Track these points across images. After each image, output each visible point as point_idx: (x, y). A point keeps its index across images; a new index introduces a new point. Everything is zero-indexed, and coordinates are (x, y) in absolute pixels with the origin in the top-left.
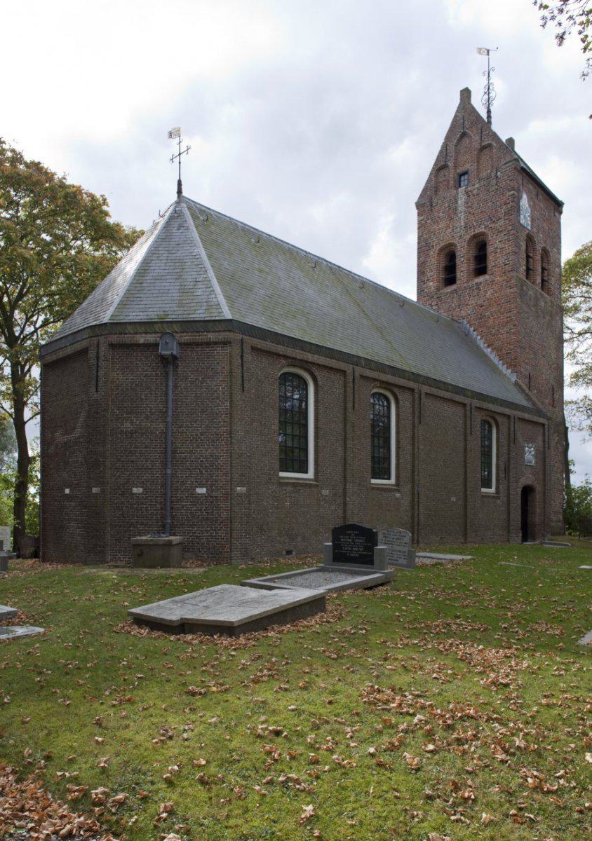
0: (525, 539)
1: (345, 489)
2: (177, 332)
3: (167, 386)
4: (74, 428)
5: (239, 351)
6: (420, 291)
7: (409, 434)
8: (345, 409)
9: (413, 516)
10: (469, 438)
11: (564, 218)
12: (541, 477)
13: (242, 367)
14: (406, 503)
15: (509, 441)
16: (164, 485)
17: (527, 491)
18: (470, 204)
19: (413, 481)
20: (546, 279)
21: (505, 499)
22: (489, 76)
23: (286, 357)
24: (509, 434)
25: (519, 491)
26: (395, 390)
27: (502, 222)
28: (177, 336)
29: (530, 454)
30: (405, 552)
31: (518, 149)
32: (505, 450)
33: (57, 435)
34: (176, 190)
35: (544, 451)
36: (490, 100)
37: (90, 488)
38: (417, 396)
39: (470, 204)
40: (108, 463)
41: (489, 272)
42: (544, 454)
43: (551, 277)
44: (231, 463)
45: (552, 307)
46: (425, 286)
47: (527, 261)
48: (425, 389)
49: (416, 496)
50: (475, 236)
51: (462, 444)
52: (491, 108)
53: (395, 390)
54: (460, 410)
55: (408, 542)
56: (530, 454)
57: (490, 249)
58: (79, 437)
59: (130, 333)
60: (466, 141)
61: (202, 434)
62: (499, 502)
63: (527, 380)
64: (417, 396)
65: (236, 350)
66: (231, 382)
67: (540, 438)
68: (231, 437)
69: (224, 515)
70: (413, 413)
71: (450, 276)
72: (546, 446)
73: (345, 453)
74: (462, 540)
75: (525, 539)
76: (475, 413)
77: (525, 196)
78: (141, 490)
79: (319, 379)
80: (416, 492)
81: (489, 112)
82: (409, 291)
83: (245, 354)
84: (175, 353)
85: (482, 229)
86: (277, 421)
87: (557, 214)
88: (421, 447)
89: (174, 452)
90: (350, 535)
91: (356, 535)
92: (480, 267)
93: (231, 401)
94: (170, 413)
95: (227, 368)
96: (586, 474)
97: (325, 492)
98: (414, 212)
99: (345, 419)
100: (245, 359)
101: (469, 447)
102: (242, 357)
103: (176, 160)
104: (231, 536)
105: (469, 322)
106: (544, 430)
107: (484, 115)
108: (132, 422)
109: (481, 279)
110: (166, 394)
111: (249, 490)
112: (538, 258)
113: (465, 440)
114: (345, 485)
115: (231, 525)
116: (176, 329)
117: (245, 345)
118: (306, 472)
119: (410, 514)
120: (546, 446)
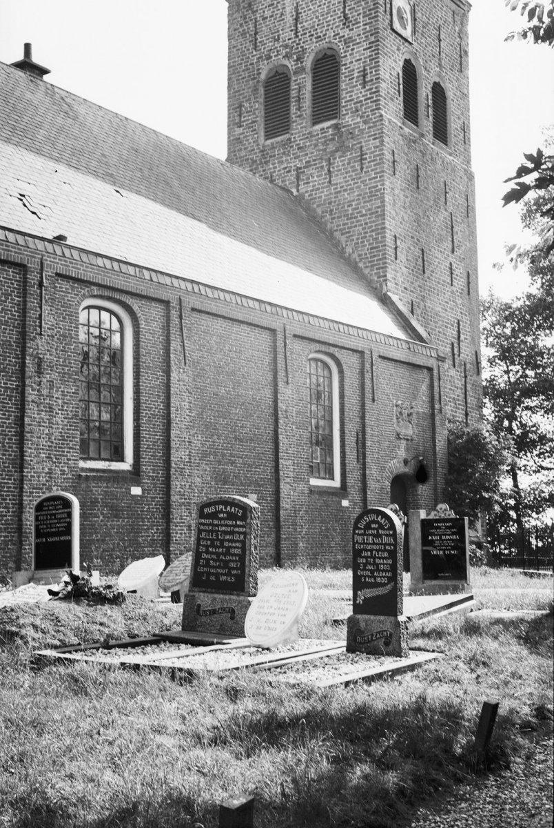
6: (234, 143)
26: (130, 301)
53: (130, 301)
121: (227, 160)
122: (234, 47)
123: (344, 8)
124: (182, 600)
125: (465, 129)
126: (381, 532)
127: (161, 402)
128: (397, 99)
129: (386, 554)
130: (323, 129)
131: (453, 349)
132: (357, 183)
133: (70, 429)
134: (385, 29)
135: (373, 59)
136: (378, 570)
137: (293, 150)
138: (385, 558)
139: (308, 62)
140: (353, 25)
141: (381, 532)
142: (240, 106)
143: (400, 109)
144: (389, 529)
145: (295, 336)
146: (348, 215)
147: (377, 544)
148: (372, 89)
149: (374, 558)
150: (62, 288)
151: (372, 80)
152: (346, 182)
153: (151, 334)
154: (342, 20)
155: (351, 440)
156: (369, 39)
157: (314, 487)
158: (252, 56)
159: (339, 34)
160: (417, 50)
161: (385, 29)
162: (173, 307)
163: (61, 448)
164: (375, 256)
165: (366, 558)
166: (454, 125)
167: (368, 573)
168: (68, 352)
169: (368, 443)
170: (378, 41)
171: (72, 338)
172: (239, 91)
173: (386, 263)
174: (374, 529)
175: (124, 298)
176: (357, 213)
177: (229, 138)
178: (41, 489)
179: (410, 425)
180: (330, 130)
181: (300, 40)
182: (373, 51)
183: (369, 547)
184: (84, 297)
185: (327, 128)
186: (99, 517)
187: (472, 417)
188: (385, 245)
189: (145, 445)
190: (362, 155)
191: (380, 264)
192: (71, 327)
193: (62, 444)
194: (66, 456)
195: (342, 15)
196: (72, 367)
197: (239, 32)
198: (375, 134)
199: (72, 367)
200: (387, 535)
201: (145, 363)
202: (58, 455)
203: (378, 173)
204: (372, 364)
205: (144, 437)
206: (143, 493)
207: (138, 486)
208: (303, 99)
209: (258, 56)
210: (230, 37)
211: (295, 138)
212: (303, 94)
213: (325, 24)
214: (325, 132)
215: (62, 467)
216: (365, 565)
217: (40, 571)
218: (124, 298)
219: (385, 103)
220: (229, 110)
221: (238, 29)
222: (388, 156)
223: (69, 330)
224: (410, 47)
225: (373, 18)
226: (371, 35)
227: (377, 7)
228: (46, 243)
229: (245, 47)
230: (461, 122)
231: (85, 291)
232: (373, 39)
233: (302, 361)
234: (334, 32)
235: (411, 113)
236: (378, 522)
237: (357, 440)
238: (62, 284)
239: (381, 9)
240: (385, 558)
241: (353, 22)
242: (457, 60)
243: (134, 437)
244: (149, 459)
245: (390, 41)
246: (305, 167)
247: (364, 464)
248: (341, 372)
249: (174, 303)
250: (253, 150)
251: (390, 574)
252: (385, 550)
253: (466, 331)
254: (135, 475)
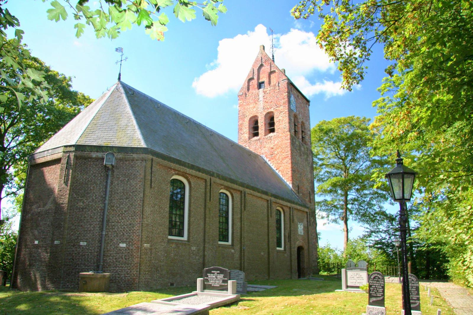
0: (299, 277)
1: (204, 247)
2: (115, 153)
3: (107, 182)
4: (46, 204)
5: (150, 165)
7: (239, 216)
8: (205, 201)
9: (241, 263)
10: (270, 218)
11: (311, 108)
12: (307, 241)
13: (151, 174)
14: (237, 256)
15: (290, 221)
16: (100, 241)
17: (300, 249)
18: (265, 97)
19: (241, 243)
20: (304, 136)
21: (289, 254)
23: (175, 170)
24: (290, 218)
25: (296, 249)
27: (282, 108)
28: (115, 155)
29: (301, 228)
30: (241, 284)
32: (288, 226)
33: (34, 207)
34: (118, 78)
35: (308, 226)
37: (53, 241)
38: (243, 195)
39: (265, 97)
40: (66, 226)
41: (276, 131)
42: (308, 228)
43: (306, 136)
44: (142, 229)
45: (307, 151)
46: (242, 136)
47: (295, 127)
48: (247, 191)
49: (243, 251)
50: (268, 113)
51: (266, 222)
55: (243, 277)
56: (301, 228)
57: (276, 120)
58: (49, 210)
59: (88, 151)
60: (263, 68)
61: (125, 211)
62: (286, 255)
63: (297, 188)
64: (243, 195)
65: (149, 163)
66: (145, 182)
67: (305, 220)
68: (143, 214)
69: (136, 260)
70: (241, 204)
72: (309, 224)
73: (205, 225)
74: (267, 277)
75: (299, 277)
77: (292, 96)
78: (85, 243)
80: (243, 250)
81: (273, 56)
83: (153, 167)
84: (113, 164)
85: (272, 110)
86: (168, 206)
87: (307, 106)
88: (245, 224)
89: (108, 221)
90: (214, 273)
91: (218, 273)
92: (271, 126)
93: (144, 194)
94: (107, 198)
95: (143, 174)
96: (75, 77)
97: (194, 248)
99: (205, 206)
100: (153, 170)
101: (270, 224)
102: (151, 168)
103: (120, 63)
104: (140, 273)
105: (266, 156)
106: (307, 215)
108: (83, 202)
109: (272, 134)
110: (106, 187)
111: (151, 246)
112: (300, 126)
113: (268, 220)
114: (204, 245)
115: (140, 267)
116: (115, 151)
117: (153, 162)
118: (183, 236)
119: (239, 262)
120: (309, 224)
124: (223, 284)
126: (379, 280)
129: (381, 287)
136: (378, 292)
141: (379, 280)
144: (382, 279)
149: (377, 288)
183: (375, 284)
204: (210, 185)
216: (373, 290)
248: (284, 211)
251: (382, 294)
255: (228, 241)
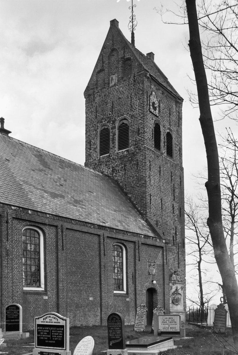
6: (88, 156)
22: (132, 10)
26: (42, 226)
31: (156, 61)
36: (134, 26)
52: (134, 31)
53: (42, 226)
54: (96, 239)
71: (105, 148)
76: (109, 241)
79: (46, 231)
81: (133, 34)
82: (80, 158)
98: (83, 100)
107: (129, 40)
121: (86, 165)
122: (88, 117)
123: (131, 103)
125: (180, 150)
127: (55, 264)
128: (152, 140)
130: (123, 152)
131: (173, 238)
132: (135, 174)
133: (19, 276)
134: (147, 111)
135: (142, 124)
136: (116, 334)
137: (111, 160)
138: (119, 330)
139: (117, 125)
140: (134, 110)
141: (117, 321)
142: (90, 142)
143: (153, 144)
145: (108, 237)
146: (132, 186)
147: (115, 325)
148: (141, 136)
150: (15, 223)
151: (141, 132)
152: (131, 173)
153: (51, 238)
154: (130, 108)
155: (130, 276)
156: (140, 116)
157: (115, 293)
158: (95, 121)
159: (129, 113)
160: (160, 119)
161: (147, 111)
162: (59, 228)
163: (16, 283)
164: (142, 203)
165: (112, 330)
166: (175, 149)
167: (113, 335)
168: (18, 247)
169: (137, 277)
170: (144, 116)
171: (19, 241)
172: (90, 135)
173: (146, 205)
174: (114, 320)
175: (39, 225)
176: (136, 186)
177: (86, 154)
178: (9, 298)
179: (154, 269)
180: (125, 152)
181: (114, 115)
182: (142, 121)
184: (24, 226)
185: (124, 151)
186: (31, 308)
187: (181, 264)
188: (146, 199)
189: (49, 280)
190: (137, 163)
191: (144, 206)
192: (19, 237)
193: (17, 281)
194: (18, 286)
195: (130, 105)
196: (20, 252)
197: (90, 111)
198: (143, 154)
199: (20, 252)
200: (118, 322)
201: (48, 249)
202: (15, 285)
203: (144, 170)
205: (48, 278)
206: (48, 298)
207: (46, 296)
208: (115, 139)
209: (97, 121)
210: (86, 113)
211: (111, 155)
212: (115, 138)
213: (124, 109)
214: (123, 153)
215: (17, 290)
217: (7, 332)
218: (39, 225)
219: (147, 142)
220: (86, 143)
221: (90, 110)
222: (148, 163)
223: (18, 238)
224: (157, 118)
225: (142, 107)
226: (141, 114)
227: (144, 103)
228: (8, 206)
229: (92, 117)
230: (179, 148)
231: (24, 223)
232: (142, 116)
233: (110, 246)
234: (127, 112)
235: (157, 145)
236: (115, 318)
237: (133, 276)
238: (15, 221)
239: (145, 103)
240: (119, 330)
241: (134, 109)
242: (177, 122)
243: (44, 278)
244: (50, 286)
245: (149, 116)
246: (115, 167)
247: (135, 285)
249: (59, 227)
250: (96, 159)
252: (118, 327)
253: (179, 231)
254: (45, 292)
255: (40, 286)
